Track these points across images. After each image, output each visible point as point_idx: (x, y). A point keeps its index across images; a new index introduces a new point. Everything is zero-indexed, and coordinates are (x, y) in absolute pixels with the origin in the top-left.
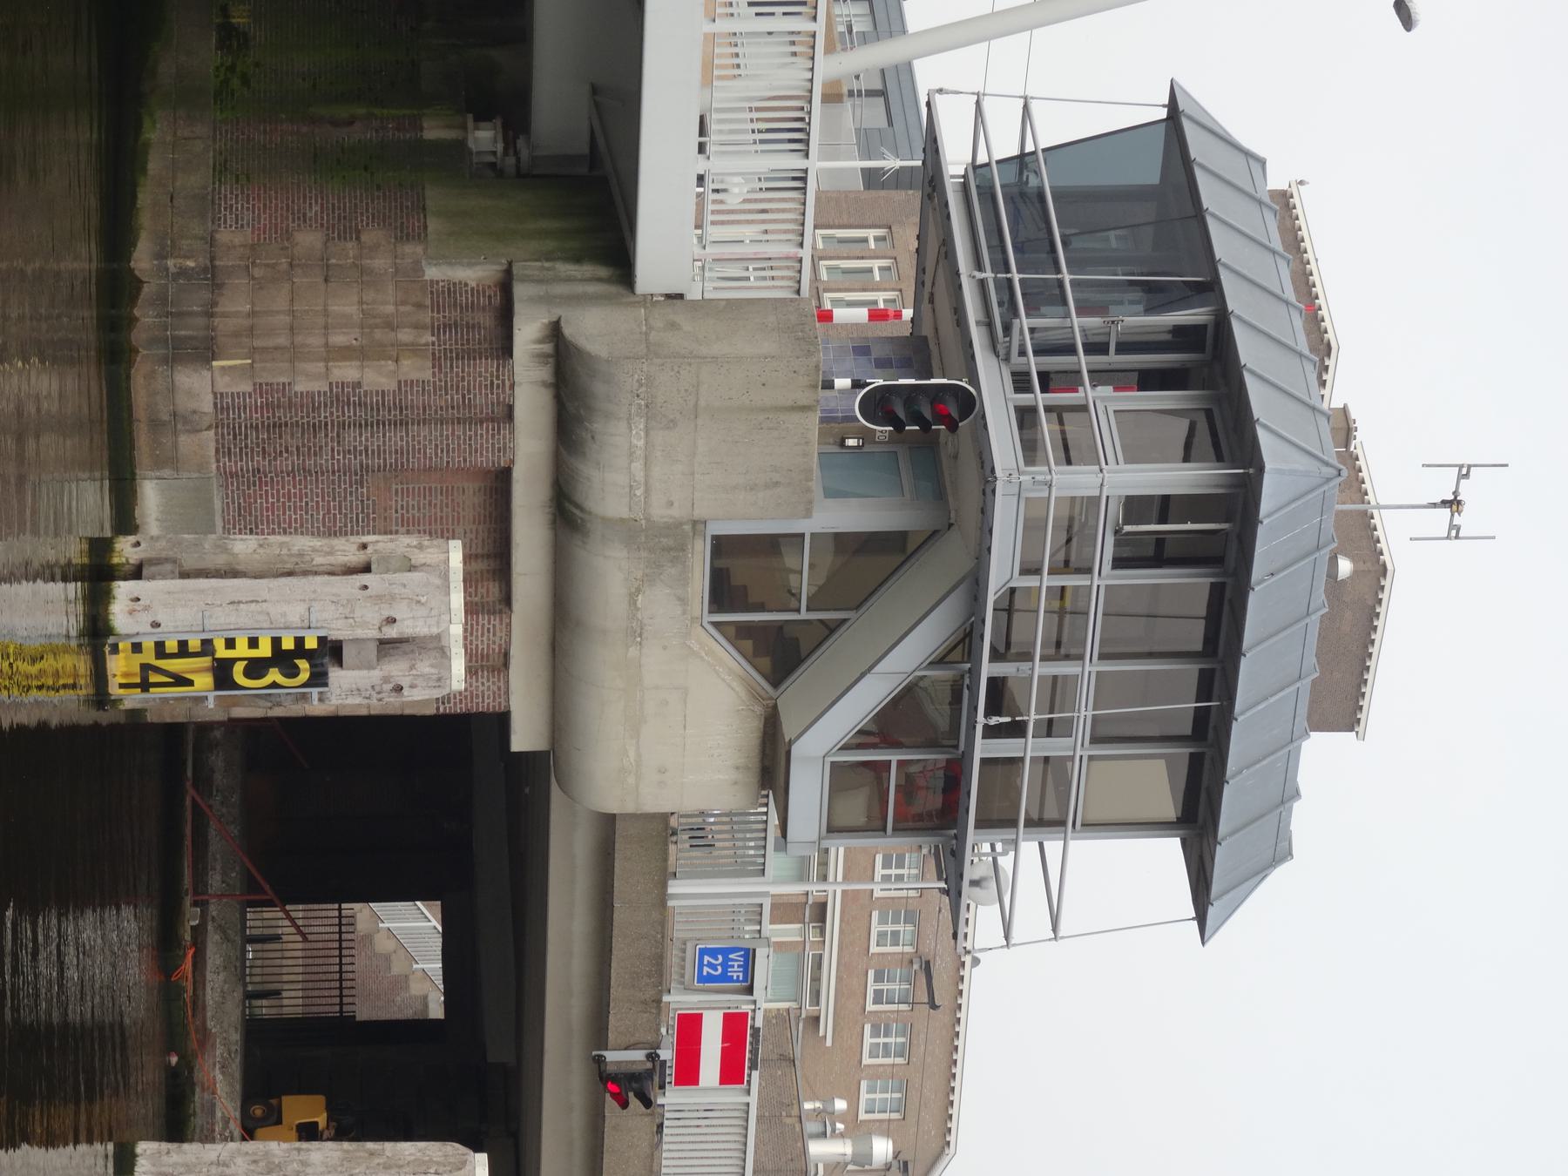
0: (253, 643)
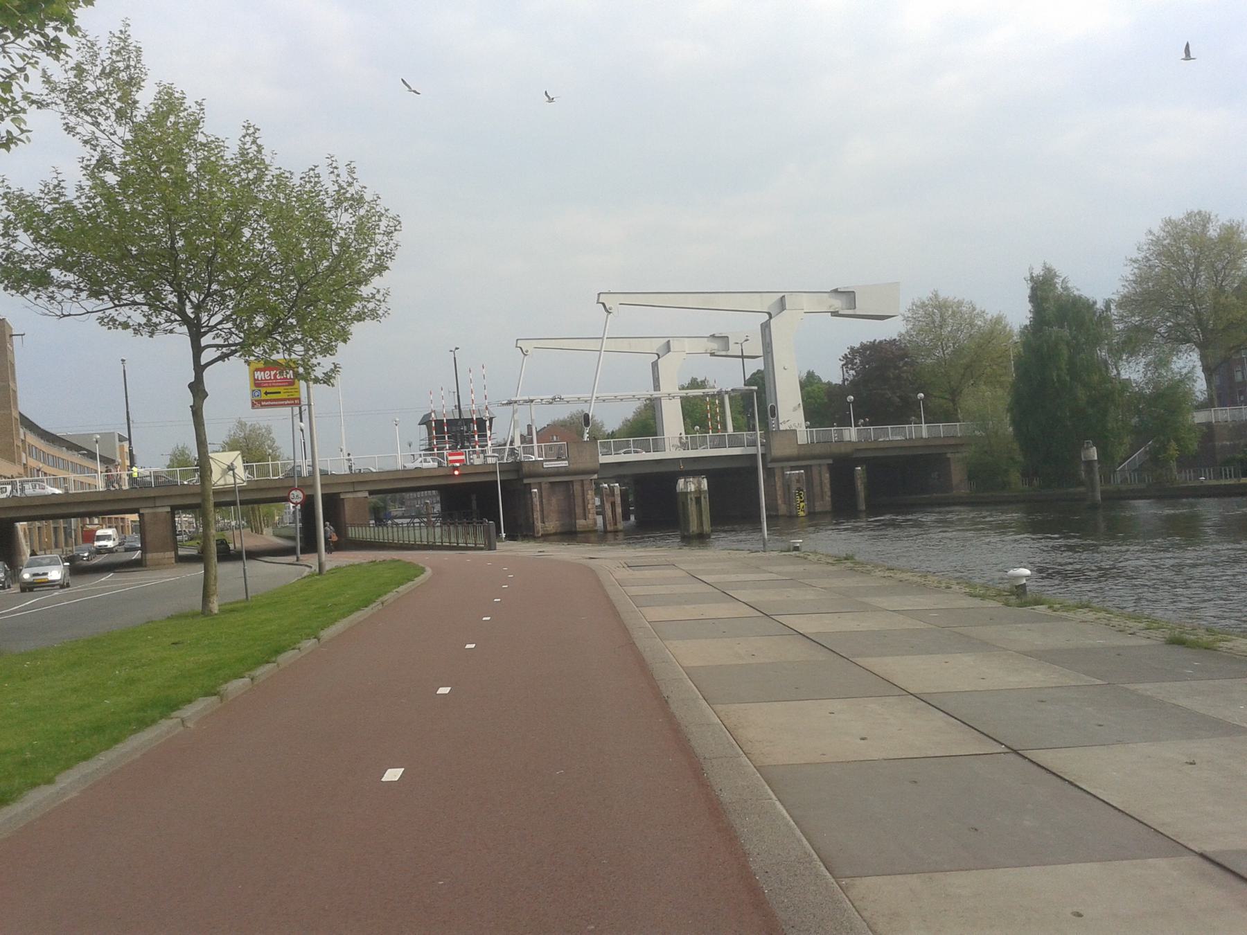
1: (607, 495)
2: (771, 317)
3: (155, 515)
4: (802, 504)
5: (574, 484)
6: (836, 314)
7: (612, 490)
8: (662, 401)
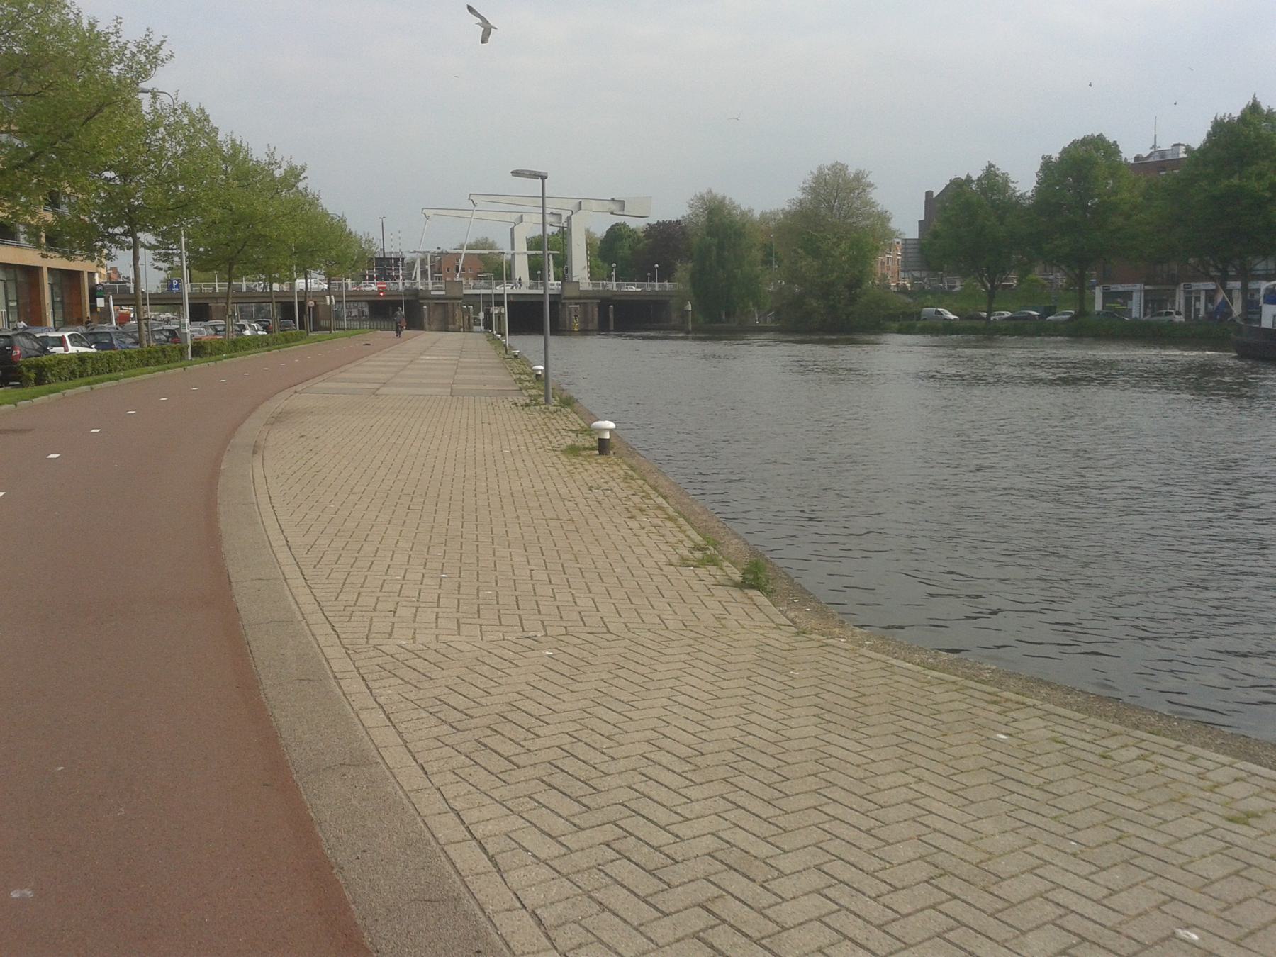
3: (217, 307)
7: (469, 309)
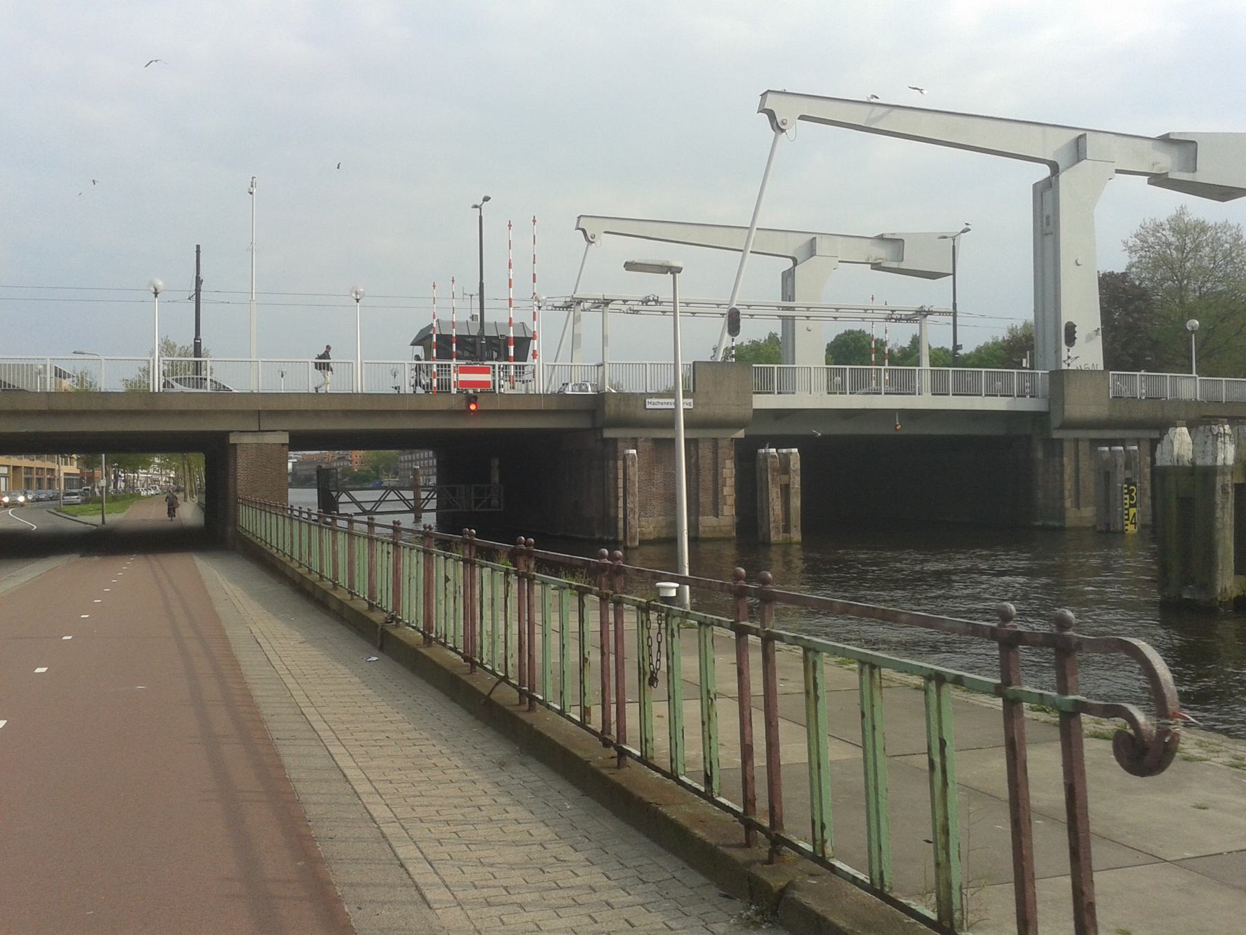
0: (1126, 499)
1: (774, 470)
2: (795, 263)
4: (1133, 511)
5: (701, 445)
6: (877, 266)
8: (796, 321)
